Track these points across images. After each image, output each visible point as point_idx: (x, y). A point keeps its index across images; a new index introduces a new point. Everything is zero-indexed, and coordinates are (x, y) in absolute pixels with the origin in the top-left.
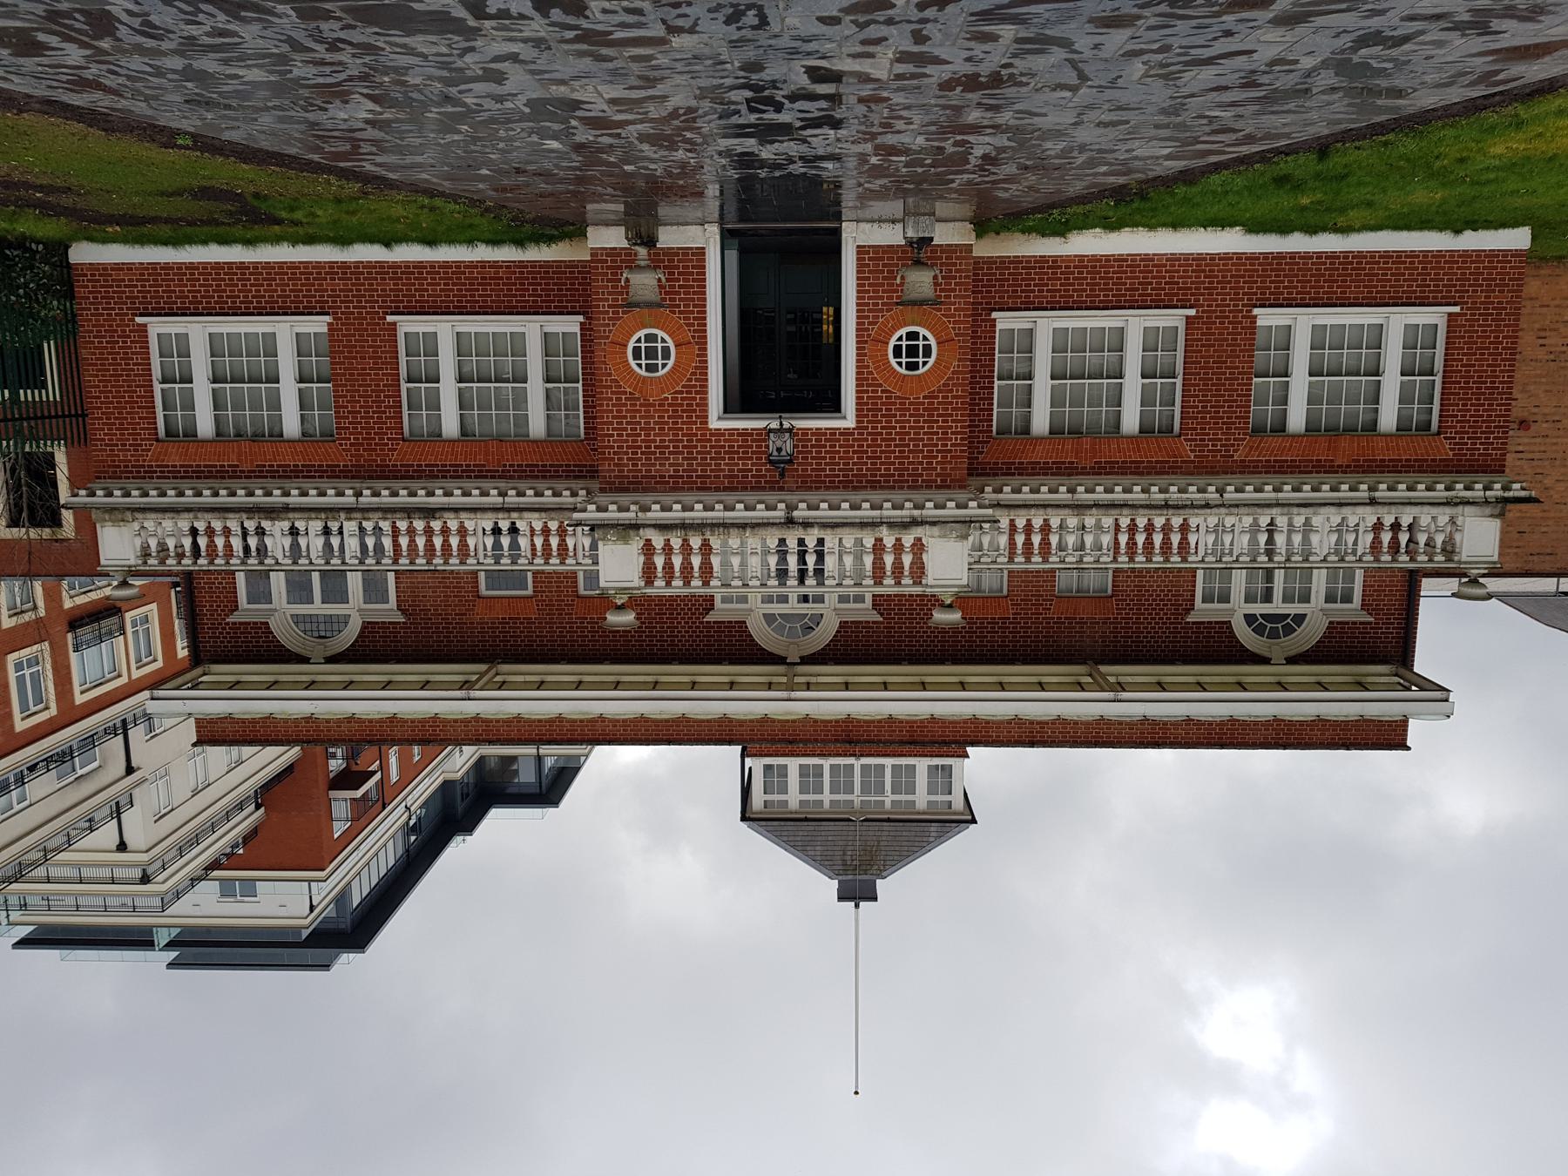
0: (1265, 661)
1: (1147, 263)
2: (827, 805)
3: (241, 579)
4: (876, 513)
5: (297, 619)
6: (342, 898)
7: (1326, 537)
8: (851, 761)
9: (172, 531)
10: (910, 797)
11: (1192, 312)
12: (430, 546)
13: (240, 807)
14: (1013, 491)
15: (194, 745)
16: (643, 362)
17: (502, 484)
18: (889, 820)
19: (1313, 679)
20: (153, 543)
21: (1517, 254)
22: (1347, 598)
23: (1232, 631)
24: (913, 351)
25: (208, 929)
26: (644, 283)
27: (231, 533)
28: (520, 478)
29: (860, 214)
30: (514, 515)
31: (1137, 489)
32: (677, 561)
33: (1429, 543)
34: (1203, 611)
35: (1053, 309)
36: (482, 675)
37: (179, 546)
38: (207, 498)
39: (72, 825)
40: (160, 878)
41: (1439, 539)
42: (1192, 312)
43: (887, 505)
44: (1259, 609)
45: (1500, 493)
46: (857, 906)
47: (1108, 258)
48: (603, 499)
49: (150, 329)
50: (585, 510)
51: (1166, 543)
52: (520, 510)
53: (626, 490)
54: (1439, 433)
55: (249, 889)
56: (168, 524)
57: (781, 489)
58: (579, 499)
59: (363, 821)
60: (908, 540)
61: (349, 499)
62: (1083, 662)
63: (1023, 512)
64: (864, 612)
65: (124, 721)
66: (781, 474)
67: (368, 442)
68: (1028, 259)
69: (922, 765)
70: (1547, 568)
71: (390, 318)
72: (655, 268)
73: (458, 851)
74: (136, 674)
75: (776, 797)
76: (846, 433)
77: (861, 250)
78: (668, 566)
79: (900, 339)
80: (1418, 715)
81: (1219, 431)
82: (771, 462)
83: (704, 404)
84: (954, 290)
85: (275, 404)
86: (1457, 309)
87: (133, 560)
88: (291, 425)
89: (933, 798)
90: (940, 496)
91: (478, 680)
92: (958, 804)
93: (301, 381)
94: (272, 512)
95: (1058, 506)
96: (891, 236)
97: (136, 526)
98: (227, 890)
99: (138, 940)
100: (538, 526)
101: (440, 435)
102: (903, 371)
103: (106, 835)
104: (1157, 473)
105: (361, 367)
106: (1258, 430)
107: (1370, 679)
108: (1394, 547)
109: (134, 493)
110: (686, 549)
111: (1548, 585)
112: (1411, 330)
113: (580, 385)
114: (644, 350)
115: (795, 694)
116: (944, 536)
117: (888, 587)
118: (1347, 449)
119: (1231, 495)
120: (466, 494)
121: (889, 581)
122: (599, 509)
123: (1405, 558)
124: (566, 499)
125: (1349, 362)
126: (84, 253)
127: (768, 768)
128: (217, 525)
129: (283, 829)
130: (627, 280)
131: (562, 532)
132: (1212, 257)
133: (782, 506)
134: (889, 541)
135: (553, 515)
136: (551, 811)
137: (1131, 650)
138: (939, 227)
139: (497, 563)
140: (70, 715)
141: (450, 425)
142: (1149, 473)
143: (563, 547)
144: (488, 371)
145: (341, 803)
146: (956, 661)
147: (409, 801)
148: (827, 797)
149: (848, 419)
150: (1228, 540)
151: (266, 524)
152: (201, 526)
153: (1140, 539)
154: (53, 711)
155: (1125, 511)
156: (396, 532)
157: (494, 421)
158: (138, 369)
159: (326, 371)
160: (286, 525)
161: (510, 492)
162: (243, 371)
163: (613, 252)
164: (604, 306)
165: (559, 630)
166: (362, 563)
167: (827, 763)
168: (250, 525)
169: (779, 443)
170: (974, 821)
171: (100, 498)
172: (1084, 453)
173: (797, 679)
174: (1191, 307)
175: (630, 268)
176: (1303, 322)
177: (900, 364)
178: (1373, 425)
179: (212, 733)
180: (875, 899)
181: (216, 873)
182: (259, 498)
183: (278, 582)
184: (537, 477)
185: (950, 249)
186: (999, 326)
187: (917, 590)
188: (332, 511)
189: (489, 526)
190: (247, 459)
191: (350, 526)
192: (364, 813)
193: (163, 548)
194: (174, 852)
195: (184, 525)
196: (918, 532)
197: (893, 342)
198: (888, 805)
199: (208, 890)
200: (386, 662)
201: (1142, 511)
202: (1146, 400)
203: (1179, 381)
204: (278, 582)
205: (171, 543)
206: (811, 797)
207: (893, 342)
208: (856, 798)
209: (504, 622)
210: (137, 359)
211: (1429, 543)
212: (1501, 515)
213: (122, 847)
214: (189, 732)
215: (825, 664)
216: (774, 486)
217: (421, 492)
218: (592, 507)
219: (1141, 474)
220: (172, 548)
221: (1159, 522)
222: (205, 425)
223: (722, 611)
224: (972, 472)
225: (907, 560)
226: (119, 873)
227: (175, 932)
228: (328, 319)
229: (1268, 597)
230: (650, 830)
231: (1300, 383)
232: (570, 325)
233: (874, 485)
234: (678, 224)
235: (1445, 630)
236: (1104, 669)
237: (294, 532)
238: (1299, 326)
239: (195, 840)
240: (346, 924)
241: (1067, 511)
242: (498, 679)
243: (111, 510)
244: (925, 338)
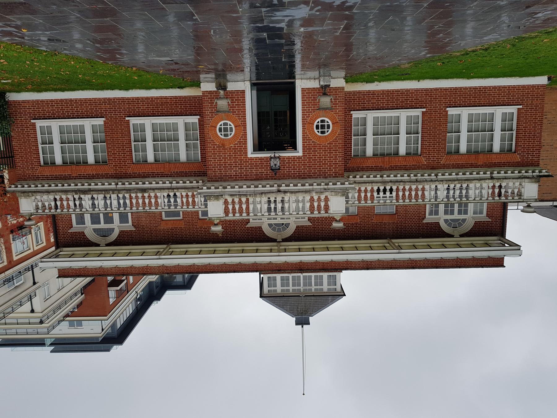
0: (452, 236)
1: (407, 92)
2: (291, 291)
3: (73, 217)
4: (311, 187)
5: (95, 230)
6: (114, 325)
7: (479, 190)
8: (299, 274)
9: (48, 200)
10: (321, 287)
11: (424, 110)
12: (144, 203)
13: (76, 294)
14: (360, 177)
15: (57, 278)
16: (223, 133)
17: (170, 179)
18: (314, 296)
19: (470, 242)
20: (40, 204)
21: (543, 86)
22: (481, 213)
23: (440, 226)
24: (323, 127)
25: (65, 339)
26: (223, 104)
27: (69, 201)
28: (177, 176)
29: (303, 77)
30: (175, 190)
31: (406, 175)
32: (237, 207)
33: (513, 193)
34: (429, 218)
35: (373, 110)
36: (165, 249)
37: (49, 205)
38: (60, 187)
39: (14, 304)
40: (47, 322)
41: (516, 191)
42: (424, 110)
43: (315, 184)
44: (449, 217)
45: (538, 174)
46: (302, 327)
47: (393, 91)
48: (209, 185)
49: (36, 124)
50: (202, 189)
51: (417, 195)
52: (178, 188)
53: (217, 181)
54: (515, 152)
55: (80, 324)
56: (45, 197)
57: (275, 179)
58: (199, 184)
59: (120, 298)
60: (323, 197)
61: (113, 186)
62: (386, 239)
63: (364, 185)
64: (305, 222)
65: (32, 266)
66: (276, 174)
67: (120, 165)
68: (364, 92)
69: (325, 275)
70: (549, 198)
71: (127, 119)
72: (227, 98)
73: (155, 307)
74: (36, 248)
75: (272, 288)
76: (299, 158)
77: (303, 90)
78: (234, 209)
79: (318, 122)
80: (509, 255)
81: (435, 154)
82: (271, 169)
83: (246, 148)
84: (338, 104)
85: (84, 151)
86: (521, 107)
87: (33, 211)
88: (91, 159)
89: (330, 287)
90: (334, 180)
91: (163, 251)
92: (339, 289)
93: (94, 143)
94: (85, 192)
95: (377, 182)
96: (315, 84)
97: (33, 198)
98: (71, 324)
99: (40, 343)
100: (184, 194)
101: (55, 164)
102: (319, 134)
103: (27, 307)
104: (413, 169)
105: (116, 136)
106: (450, 153)
107: (490, 242)
108: (500, 195)
109: (32, 186)
110: (240, 202)
111: (550, 203)
112: (504, 114)
113: (199, 142)
114: (223, 129)
115: (281, 254)
116: (336, 195)
117: (316, 214)
118: (482, 159)
119: (440, 177)
120: (157, 183)
121: (316, 212)
122: (208, 188)
123: (504, 198)
124: (195, 184)
125: (483, 127)
126: (13, 97)
127: (269, 278)
128: (64, 197)
129: (92, 301)
130: (216, 103)
131: (193, 196)
132: (431, 89)
133: (276, 185)
134: (316, 198)
135: (190, 190)
136: (188, 291)
137: (401, 234)
138: (332, 80)
139: (169, 208)
140: (11, 264)
141: (151, 158)
142: (410, 170)
143: (194, 201)
144: (164, 137)
145: (112, 292)
146: (339, 239)
147: (137, 290)
148: (291, 288)
149: (299, 153)
150: (435, 194)
151: (82, 196)
152: (58, 197)
153: (407, 193)
154: (5, 263)
155: (402, 184)
156: (131, 198)
157: (166, 155)
158: (33, 140)
159: (103, 138)
160: (90, 196)
161: (174, 182)
162: (73, 139)
163: (210, 92)
164: (207, 113)
165: (193, 233)
166: (119, 209)
167: (291, 276)
168: (76, 197)
169: (275, 162)
170: (345, 295)
171: (19, 188)
172: (386, 162)
173: (281, 248)
174: (424, 108)
175: (217, 98)
176: (465, 113)
177: (318, 132)
178: (491, 150)
179: (63, 274)
180: (309, 324)
181: (68, 318)
182: (80, 187)
183: (87, 217)
184: (183, 176)
185: (336, 89)
186: (353, 116)
187: (327, 215)
188: (106, 191)
189: (166, 194)
190: (74, 172)
191: (114, 196)
192: (121, 295)
193: (44, 206)
194: (52, 312)
195: (51, 197)
196: (327, 194)
197: (316, 124)
198: (313, 290)
199: (65, 325)
200: (128, 245)
201: (407, 183)
202: (408, 142)
203: (420, 135)
204: (87, 217)
205: (47, 204)
206: (285, 288)
207: (316, 124)
208: (302, 288)
209: (172, 229)
210: (32, 136)
211: (513, 193)
212: (539, 182)
213: (32, 311)
214: (56, 273)
215: (291, 241)
216: (272, 178)
217: (140, 183)
218: (205, 188)
219: (407, 170)
220: (47, 206)
221: (414, 187)
222: (59, 160)
223: (253, 223)
224: (346, 170)
225: (323, 204)
226: (31, 321)
227: (53, 340)
228: (104, 119)
229: (452, 213)
230: (227, 301)
231: (464, 135)
232: (194, 119)
233: (310, 177)
234: (235, 81)
235: (520, 224)
236: (394, 241)
237: (93, 198)
238: (463, 114)
239: (59, 307)
240: (115, 335)
241: (380, 184)
242: (170, 250)
243: (24, 192)
244: (327, 122)
